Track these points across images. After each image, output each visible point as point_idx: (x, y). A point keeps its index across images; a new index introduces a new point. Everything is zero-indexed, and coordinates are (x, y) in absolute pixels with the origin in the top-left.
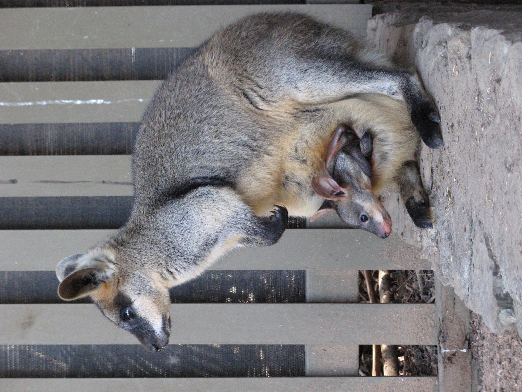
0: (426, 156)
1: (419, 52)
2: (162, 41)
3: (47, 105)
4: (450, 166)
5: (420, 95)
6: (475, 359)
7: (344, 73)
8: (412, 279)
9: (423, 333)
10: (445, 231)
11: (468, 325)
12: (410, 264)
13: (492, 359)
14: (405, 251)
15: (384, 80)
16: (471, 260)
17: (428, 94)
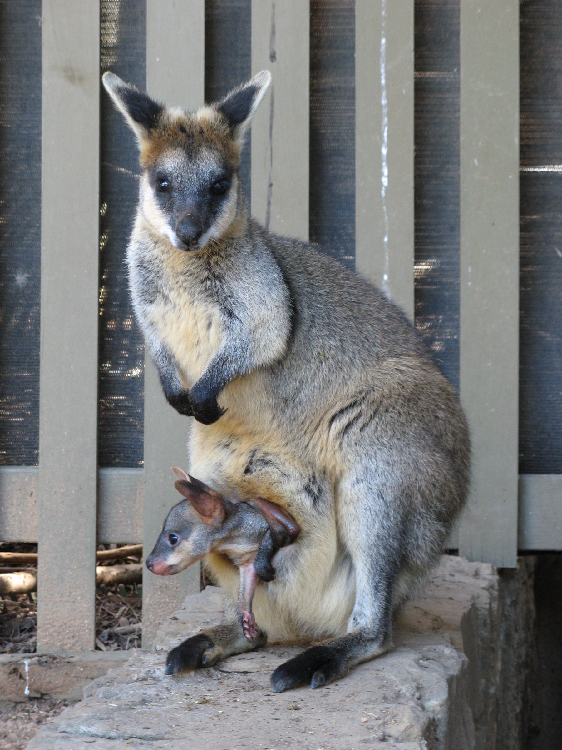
0: (267, 664)
1: (413, 655)
2: (470, 271)
3: (381, 106)
4: (243, 703)
5: (350, 658)
6: (15, 707)
7: (383, 552)
8: (133, 616)
9: (54, 634)
10: (155, 693)
11: (62, 697)
12: (151, 616)
13: (5, 736)
14: (169, 609)
15: (374, 607)
16: (103, 737)
17: (351, 669)
